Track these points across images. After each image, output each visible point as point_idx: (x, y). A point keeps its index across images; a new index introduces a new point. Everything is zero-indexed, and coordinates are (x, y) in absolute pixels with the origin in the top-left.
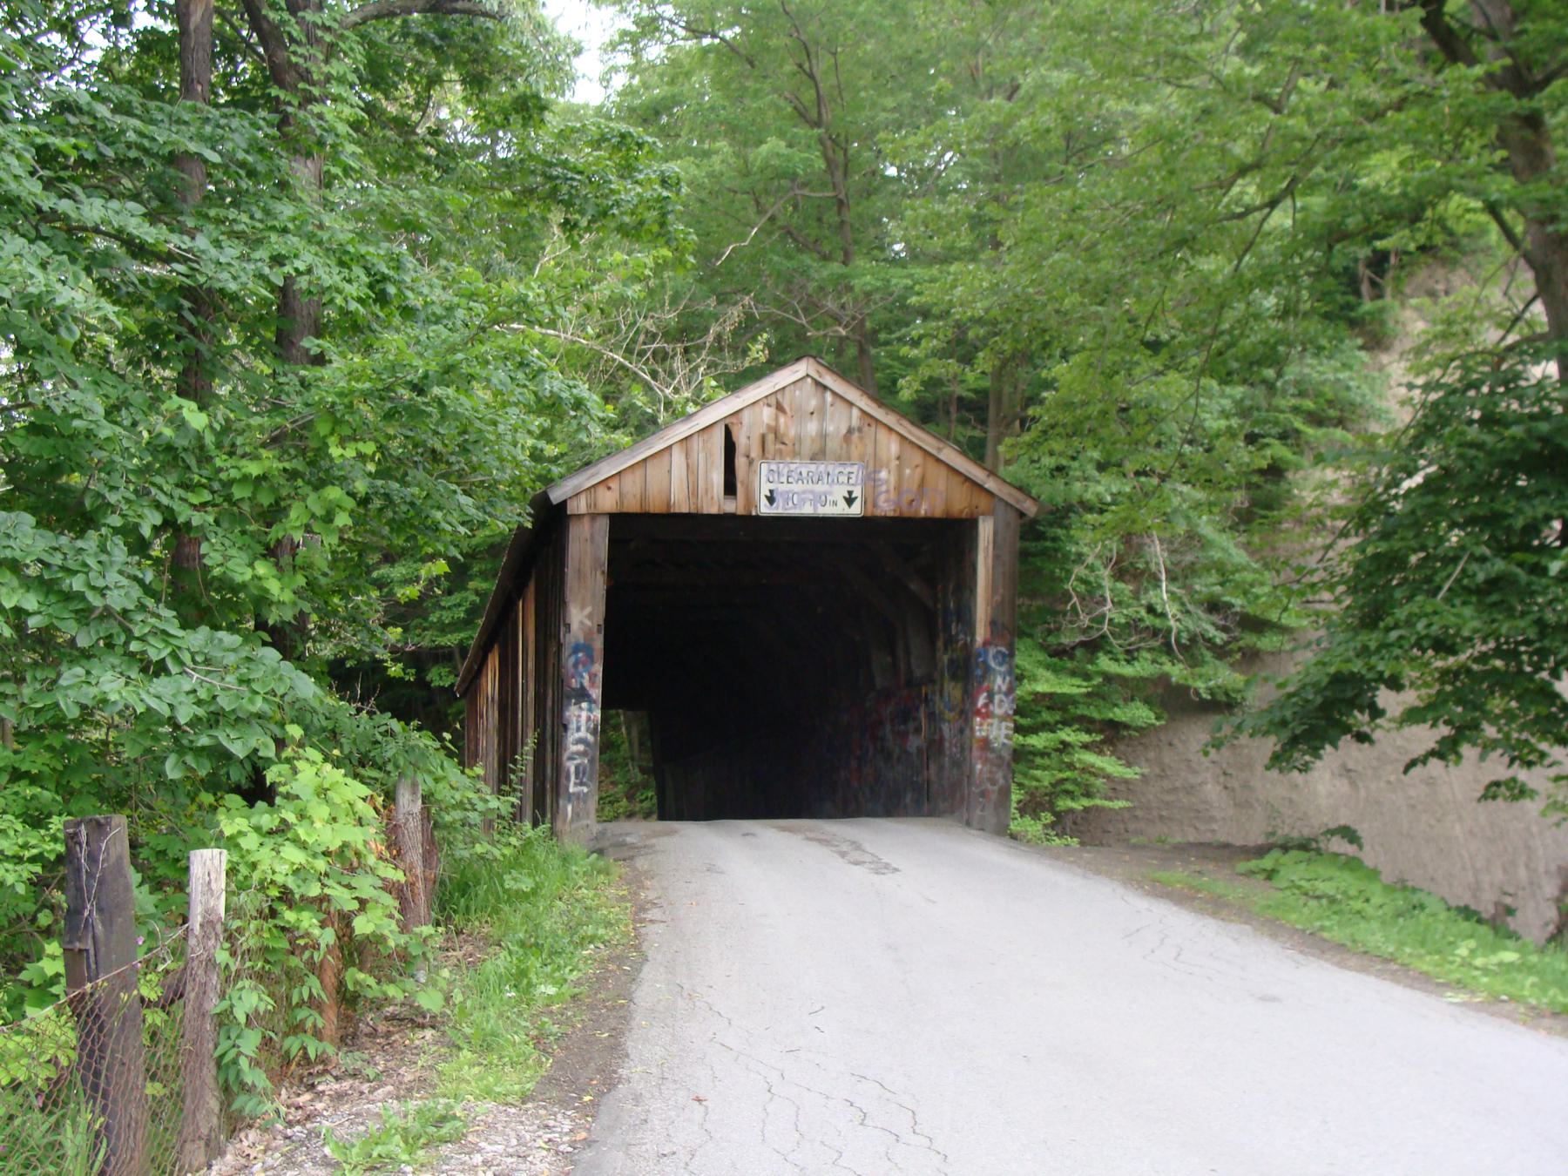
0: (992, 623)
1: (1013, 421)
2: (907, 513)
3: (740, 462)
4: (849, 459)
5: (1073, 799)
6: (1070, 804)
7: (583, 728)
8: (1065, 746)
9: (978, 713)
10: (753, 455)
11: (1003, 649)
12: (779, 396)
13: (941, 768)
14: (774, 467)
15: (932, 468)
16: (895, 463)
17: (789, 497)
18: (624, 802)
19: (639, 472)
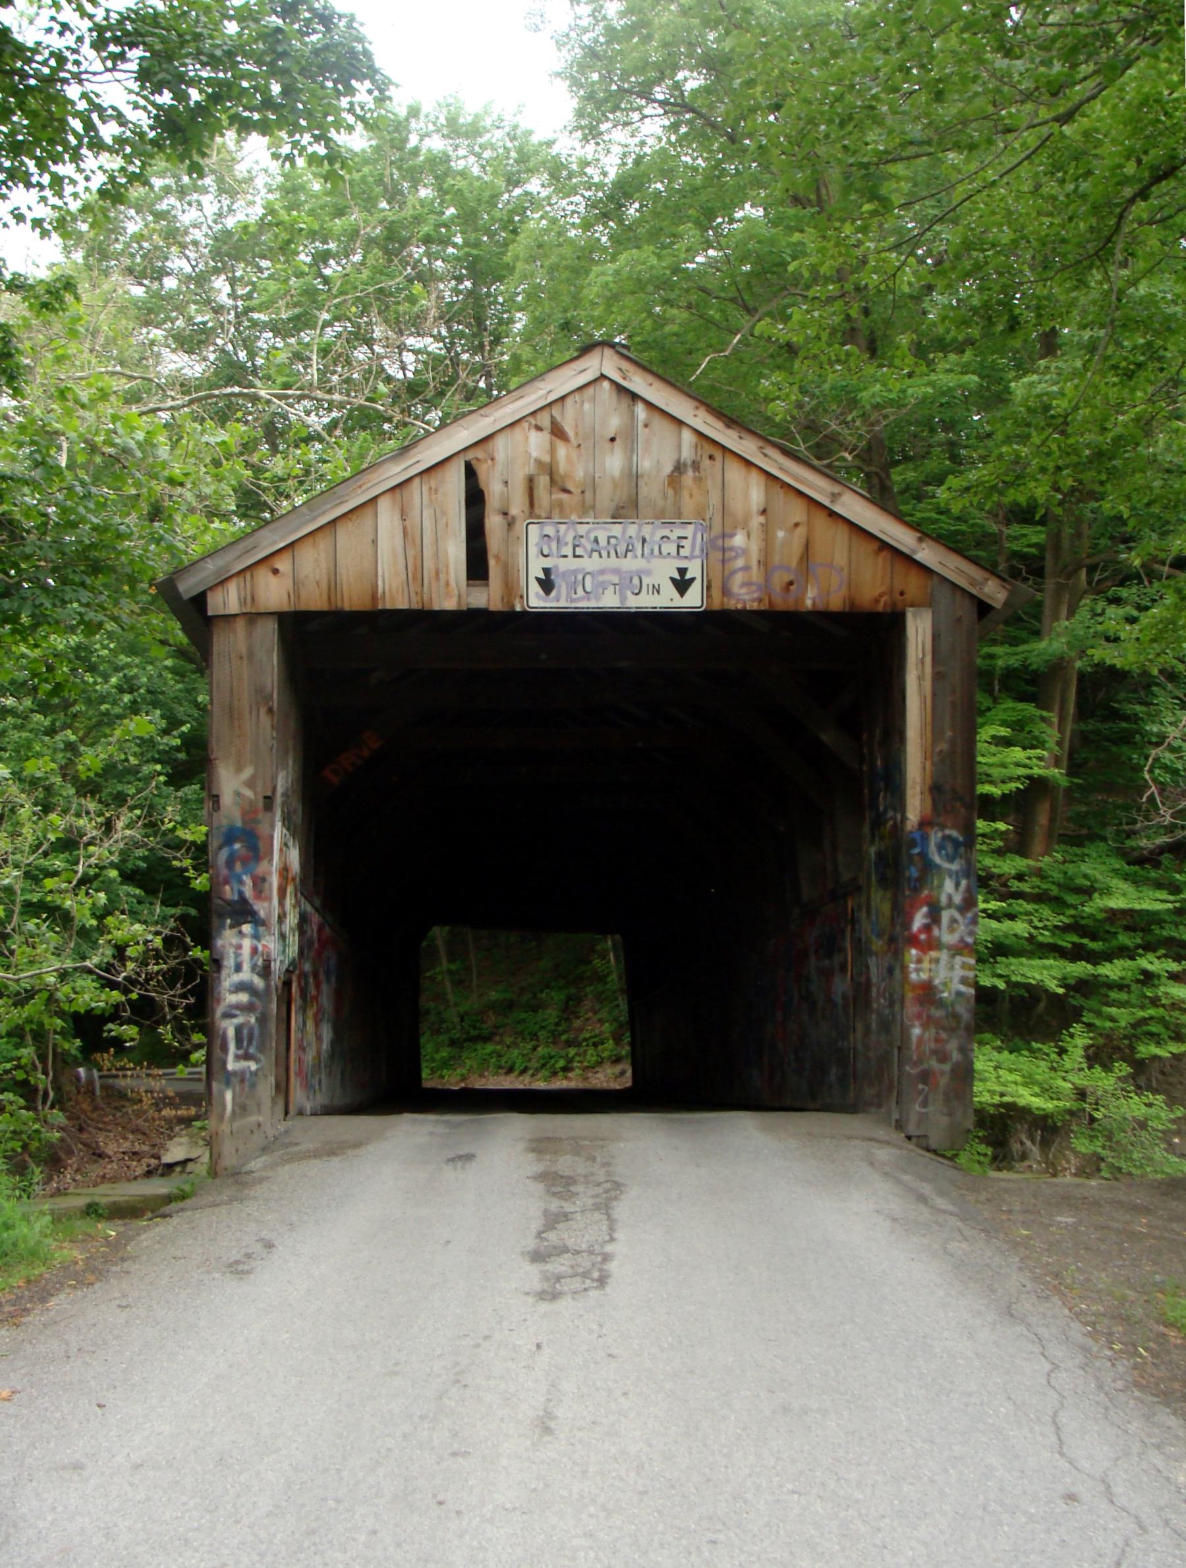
0: (935, 789)
1: (1077, 570)
2: (781, 604)
3: (493, 523)
4: (679, 515)
5: (1158, 1044)
6: (1154, 1050)
7: (246, 967)
8: (1148, 978)
9: (913, 941)
10: (514, 511)
11: (955, 833)
12: (556, 411)
13: (867, 1031)
14: (549, 530)
15: (822, 526)
16: (757, 521)
17: (576, 580)
18: (610, 1044)
19: (323, 543)
